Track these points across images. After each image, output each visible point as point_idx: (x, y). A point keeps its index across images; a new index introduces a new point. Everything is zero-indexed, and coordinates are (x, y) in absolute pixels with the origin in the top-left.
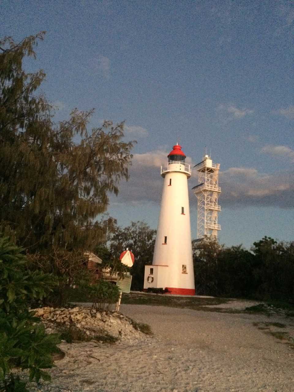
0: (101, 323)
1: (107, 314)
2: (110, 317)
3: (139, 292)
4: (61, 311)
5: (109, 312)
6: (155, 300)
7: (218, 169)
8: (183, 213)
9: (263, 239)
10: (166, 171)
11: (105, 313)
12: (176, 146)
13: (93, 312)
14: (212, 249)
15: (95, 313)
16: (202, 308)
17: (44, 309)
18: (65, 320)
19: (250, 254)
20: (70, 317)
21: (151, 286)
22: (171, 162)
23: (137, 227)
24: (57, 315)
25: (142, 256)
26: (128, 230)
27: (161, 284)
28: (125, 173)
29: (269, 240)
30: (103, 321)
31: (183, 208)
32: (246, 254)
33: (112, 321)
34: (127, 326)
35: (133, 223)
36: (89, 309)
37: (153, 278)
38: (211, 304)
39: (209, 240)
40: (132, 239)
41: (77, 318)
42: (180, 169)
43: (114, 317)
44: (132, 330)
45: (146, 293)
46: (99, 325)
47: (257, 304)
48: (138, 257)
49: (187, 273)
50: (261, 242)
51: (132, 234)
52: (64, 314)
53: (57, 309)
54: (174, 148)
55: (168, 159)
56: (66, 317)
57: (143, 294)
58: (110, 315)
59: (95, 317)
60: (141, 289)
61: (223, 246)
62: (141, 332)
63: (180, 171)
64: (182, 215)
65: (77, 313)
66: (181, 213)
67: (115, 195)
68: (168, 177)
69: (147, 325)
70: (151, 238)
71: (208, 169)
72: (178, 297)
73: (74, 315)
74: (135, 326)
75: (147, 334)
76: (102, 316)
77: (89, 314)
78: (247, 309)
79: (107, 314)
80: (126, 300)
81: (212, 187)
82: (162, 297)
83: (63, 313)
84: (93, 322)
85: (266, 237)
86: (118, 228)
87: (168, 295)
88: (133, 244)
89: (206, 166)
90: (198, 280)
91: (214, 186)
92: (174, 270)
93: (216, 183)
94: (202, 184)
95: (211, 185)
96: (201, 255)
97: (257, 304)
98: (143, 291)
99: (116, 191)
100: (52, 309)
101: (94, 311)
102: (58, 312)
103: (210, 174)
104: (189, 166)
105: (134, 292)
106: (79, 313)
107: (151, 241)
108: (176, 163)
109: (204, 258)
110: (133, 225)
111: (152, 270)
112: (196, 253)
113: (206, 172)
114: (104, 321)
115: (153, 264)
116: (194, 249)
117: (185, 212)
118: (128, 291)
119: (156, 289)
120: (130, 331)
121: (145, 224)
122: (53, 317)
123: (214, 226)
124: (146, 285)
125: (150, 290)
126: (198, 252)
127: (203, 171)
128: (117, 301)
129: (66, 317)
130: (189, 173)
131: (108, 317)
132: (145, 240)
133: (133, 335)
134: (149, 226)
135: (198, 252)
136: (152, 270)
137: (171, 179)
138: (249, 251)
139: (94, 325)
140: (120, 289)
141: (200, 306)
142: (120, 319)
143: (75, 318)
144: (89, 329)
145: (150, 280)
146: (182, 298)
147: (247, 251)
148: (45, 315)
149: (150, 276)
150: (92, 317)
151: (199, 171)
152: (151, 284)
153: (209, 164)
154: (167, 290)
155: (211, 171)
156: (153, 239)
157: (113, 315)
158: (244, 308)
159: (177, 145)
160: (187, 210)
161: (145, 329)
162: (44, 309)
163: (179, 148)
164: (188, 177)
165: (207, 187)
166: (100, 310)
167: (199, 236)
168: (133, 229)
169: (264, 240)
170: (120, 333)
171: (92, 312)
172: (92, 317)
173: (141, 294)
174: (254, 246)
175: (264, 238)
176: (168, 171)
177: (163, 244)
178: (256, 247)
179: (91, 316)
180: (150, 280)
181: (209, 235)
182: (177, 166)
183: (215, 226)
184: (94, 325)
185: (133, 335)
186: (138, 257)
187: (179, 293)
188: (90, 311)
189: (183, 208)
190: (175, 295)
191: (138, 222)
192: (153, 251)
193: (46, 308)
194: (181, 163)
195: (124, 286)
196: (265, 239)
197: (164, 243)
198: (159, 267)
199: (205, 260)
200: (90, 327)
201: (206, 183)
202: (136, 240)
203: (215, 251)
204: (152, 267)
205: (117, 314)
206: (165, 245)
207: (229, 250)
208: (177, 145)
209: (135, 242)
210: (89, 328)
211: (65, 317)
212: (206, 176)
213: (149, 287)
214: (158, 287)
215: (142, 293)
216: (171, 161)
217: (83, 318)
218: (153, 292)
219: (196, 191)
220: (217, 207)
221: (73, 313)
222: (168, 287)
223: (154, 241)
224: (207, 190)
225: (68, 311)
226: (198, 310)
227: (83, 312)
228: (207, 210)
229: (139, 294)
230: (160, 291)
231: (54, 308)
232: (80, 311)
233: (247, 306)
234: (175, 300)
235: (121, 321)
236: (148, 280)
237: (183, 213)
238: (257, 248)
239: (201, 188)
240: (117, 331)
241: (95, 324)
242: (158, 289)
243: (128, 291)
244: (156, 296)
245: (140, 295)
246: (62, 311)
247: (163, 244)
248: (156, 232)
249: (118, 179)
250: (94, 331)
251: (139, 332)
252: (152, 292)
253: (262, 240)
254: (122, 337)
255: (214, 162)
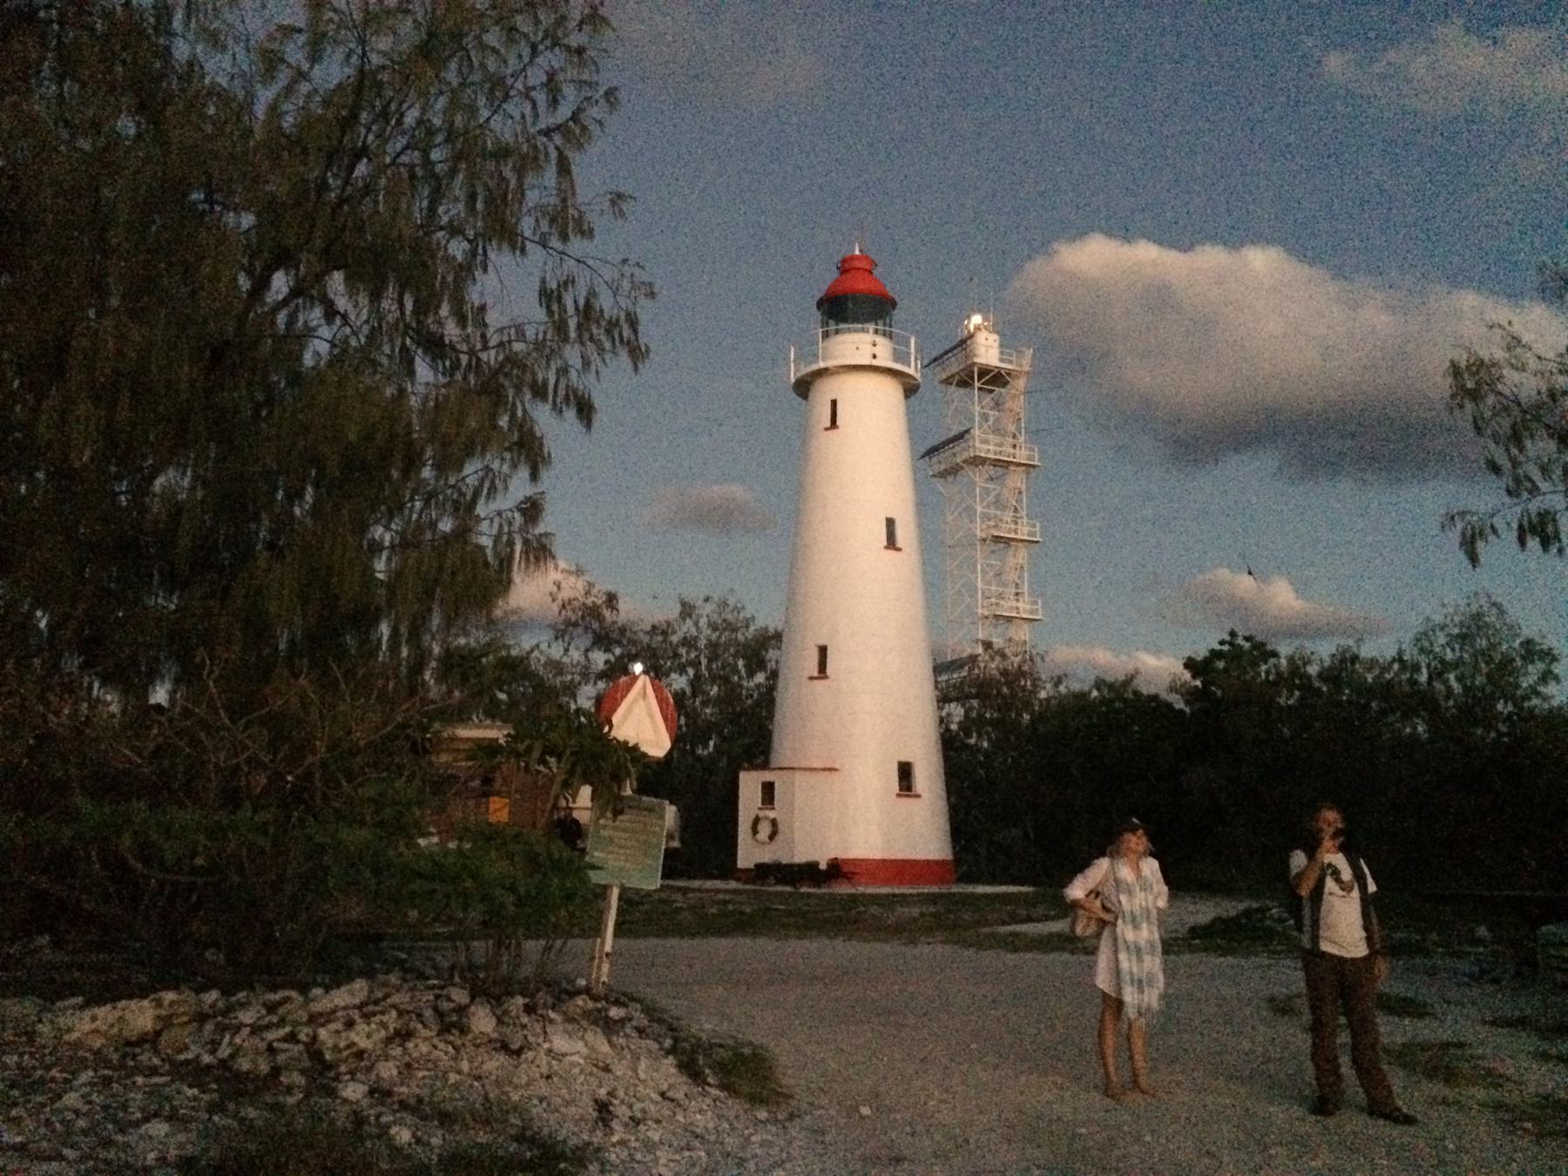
0: (495, 1064)
1: (529, 1009)
2: (551, 1021)
3: (718, 884)
4: (265, 1005)
5: (555, 992)
6: (790, 914)
7: (1027, 369)
8: (891, 543)
9: (1222, 643)
10: (814, 367)
11: (520, 1001)
12: (853, 258)
13: (449, 999)
14: (1014, 695)
15: (462, 1010)
16: (993, 936)
17: (159, 1003)
18: (281, 1058)
19: (1169, 706)
20: (315, 1038)
21: (766, 856)
22: (833, 327)
23: (703, 621)
24: (238, 1029)
25: (723, 739)
26: (664, 633)
27: (812, 842)
28: (626, 333)
29: (1247, 645)
30: (504, 1047)
31: (890, 523)
32: (1150, 708)
33: (560, 1043)
34: (643, 1064)
35: (684, 604)
36: (432, 988)
37: (774, 823)
38: (1029, 919)
39: (998, 658)
40: (682, 670)
41: (348, 1047)
42: (875, 356)
43: (570, 1019)
44: (671, 1086)
45: (748, 887)
46: (478, 1078)
47: (1230, 908)
48: (711, 743)
49: (918, 796)
50: (1216, 655)
51: (682, 651)
52: (282, 1022)
53: (242, 995)
54: (846, 266)
55: (817, 315)
56: (292, 1038)
57: (734, 892)
58: (552, 1015)
59: (464, 1030)
60: (727, 868)
61: (1058, 681)
62: (722, 1095)
63: (875, 363)
64: (891, 553)
65: (356, 1015)
66: (885, 543)
67: (579, 427)
68: (825, 391)
69: (755, 1047)
70: (761, 665)
71: (984, 371)
72: (887, 896)
73: (338, 1026)
74: (691, 1060)
75: (755, 1100)
76: (500, 1021)
77: (428, 1013)
78: (1194, 931)
79: (529, 1009)
80: (641, 916)
81: (1001, 445)
82: (820, 897)
83: (275, 1019)
84: (445, 1061)
85: (1233, 634)
86: (623, 630)
87: (843, 889)
88: (688, 691)
89: (976, 360)
90: (960, 828)
91: (1011, 440)
92: (861, 779)
93: (1019, 429)
94: (961, 436)
95: (998, 439)
96: (966, 726)
97: (1230, 908)
98: (738, 880)
99: (585, 410)
100: (212, 996)
101: (460, 996)
102: (247, 1017)
103: (991, 391)
104: (913, 341)
105: (671, 882)
106: (367, 1017)
107: (760, 678)
108: (856, 331)
109: (980, 735)
110: (687, 610)
111: (768, 789)
112: (949, 715)
113: (977, 384)
114: (515, 1046)
115: (774, 762)
116: (943, 699)
117: (900, 543)
118: (652, 882)
119: (790, 866)
120: (663, 1095)
121: (738, 610)
122: (214, 1046)
123: (1014, 604)
124: (749, 853)
125: (764, 872)
126: (957, 711)
127: (965, 382)
128: (597, 931)
129: (292, 1038)
130: (911, 371)
131: (538, 1028)
132: (736, 671)
133: (680, 1118)
134: (753, 618)
135: (957, 711)
136: (768, 789)
137: (834, 403)
138: (1164, 695)
139: (453, 1078)
140: (594, 867)
141: (986, 930)
142: (610, 1027)
143: (342, 1044)
144: (413, 1108)
145: (764, 830)
146: (904, 899)
147: (1155, 698)
148: (164, 1038)
149: (761, 814)
150: (445, 1029)
151: (947, 381)
152: (768, 848)
153: (988, 351)
154: (838, 870)
155: (995, 378)
156: (771, 665)
157: (565, 1013)
158: (1183, 931)
159: (857, 252)
160: (906, 533)
161: (743, 1073)
162: (159, 1003)
163: (864, 265)
164: (910, 390)
165: (984, 444)
166: (492, 991)
167: (964, 644)
168: (688, 627)
169: (1226, 648)
170: (604, 1109)
171: (445, 1006)
172: (445, 1029)
173: (726, 891)
174: (1187, 675)
175: (1228, 638)
176: (822, 365)
177: (811, 678)
178: (1194, 677)
179: (436, 1028)
180: (764, 830)
181: (998, 642)
182: (859, 344)
183: (1020, 605)
184: (453, 1078)
185: (680, 1118)
186: (711, 743)
187: (887, 882)
188: (437, 997)
189: (890, 523)
190: (870, 890)
191: (707, 600)
192: (771, 717)
193: (169, 996)
194: (876, 332)
195: (628, 853)
196: (1230, 644)
197: (816, 674)
198: (798, 774)
199: (985, 744)
200: (425, 1093)
201: (976, 432)
202: (697, 677)
203: (1027, 705)
204: (767, 776)
205: (591, 1005)
206: (820, 685)
207: (1082, 696)
208: (857, 252)
209: (696, 683)
210: (420, 1100)
211: (285, 1039)
212: (977, 403)
213: (759, 861)
214: (800, 857)
215: (733, 885)
216: (831, 322)
217: (388, 1041)
218: (779, 882)
219: (941, 462)
220: (1026, 529)
221: (327, 1017)
222: (842, 855)
223: (774, 675)
224: (983, 461)
225: (308, 1001)
226: (981, 946)
227: (394, 1006)
228: (984, 540)
229: (718, 891)
230: (809, 873)
231: (226, 993)
232: (376, 1002)
233: (1192, 921)
234: (874, 910)
235: (610, 1042)
236: (755, 831)
237: (891, 543)
238: (1198, 683)
239: (960, 454)
240: (587, 1100)
241: (459, 1072)
242: (799, 865)
243: (652, 882)
244: (791, 894)
245: (721, 896)
246: (271, 1008)
247: (811, 678)
248: (778, 636)
249: (594, 356)
250: (446, 1118)
251: (714, 1092)
252: (772, 880)
253: (1218, 647)
254: (615, 1139)
255: (1007, 345)
